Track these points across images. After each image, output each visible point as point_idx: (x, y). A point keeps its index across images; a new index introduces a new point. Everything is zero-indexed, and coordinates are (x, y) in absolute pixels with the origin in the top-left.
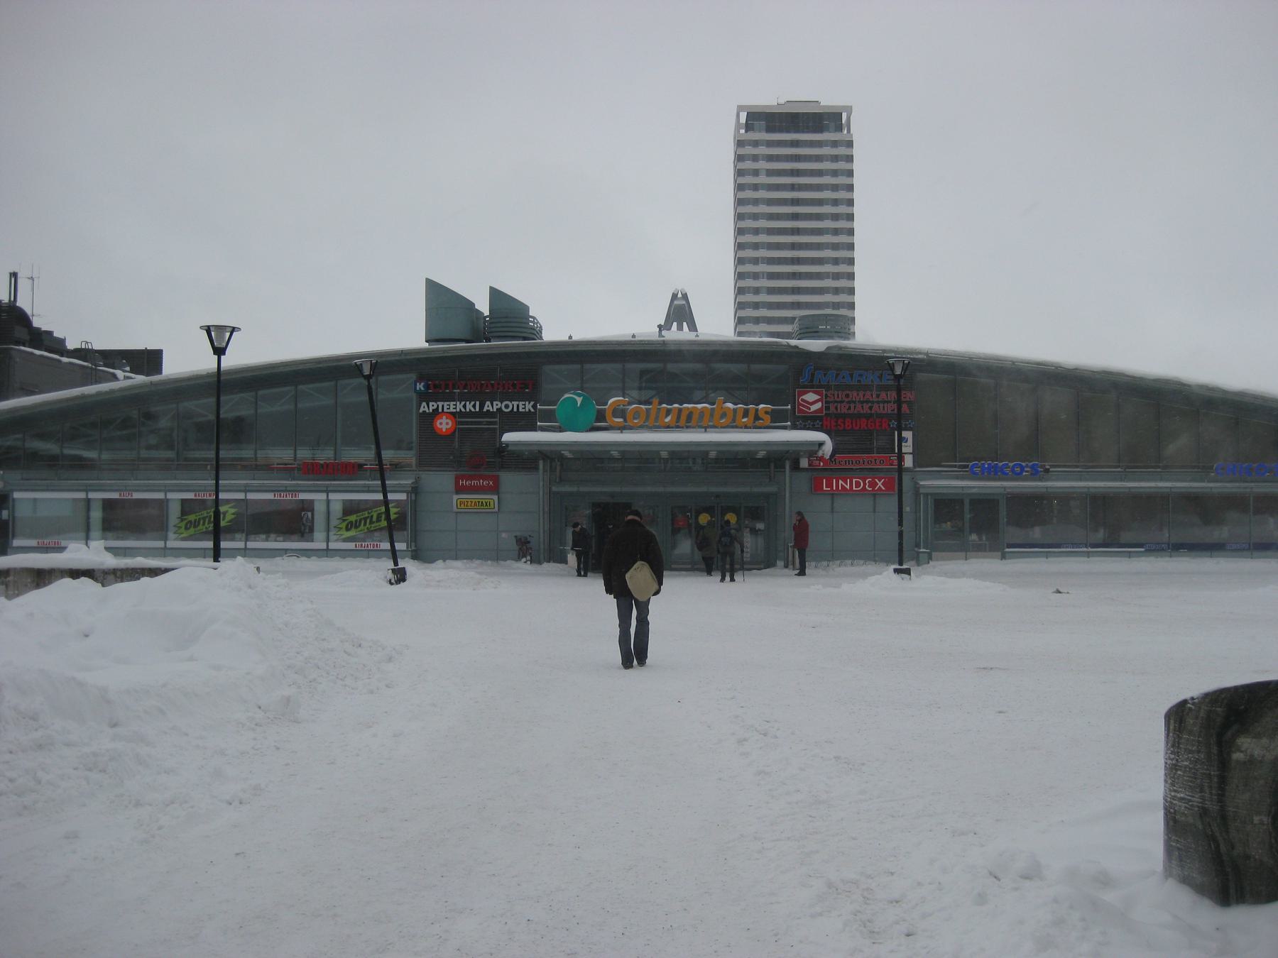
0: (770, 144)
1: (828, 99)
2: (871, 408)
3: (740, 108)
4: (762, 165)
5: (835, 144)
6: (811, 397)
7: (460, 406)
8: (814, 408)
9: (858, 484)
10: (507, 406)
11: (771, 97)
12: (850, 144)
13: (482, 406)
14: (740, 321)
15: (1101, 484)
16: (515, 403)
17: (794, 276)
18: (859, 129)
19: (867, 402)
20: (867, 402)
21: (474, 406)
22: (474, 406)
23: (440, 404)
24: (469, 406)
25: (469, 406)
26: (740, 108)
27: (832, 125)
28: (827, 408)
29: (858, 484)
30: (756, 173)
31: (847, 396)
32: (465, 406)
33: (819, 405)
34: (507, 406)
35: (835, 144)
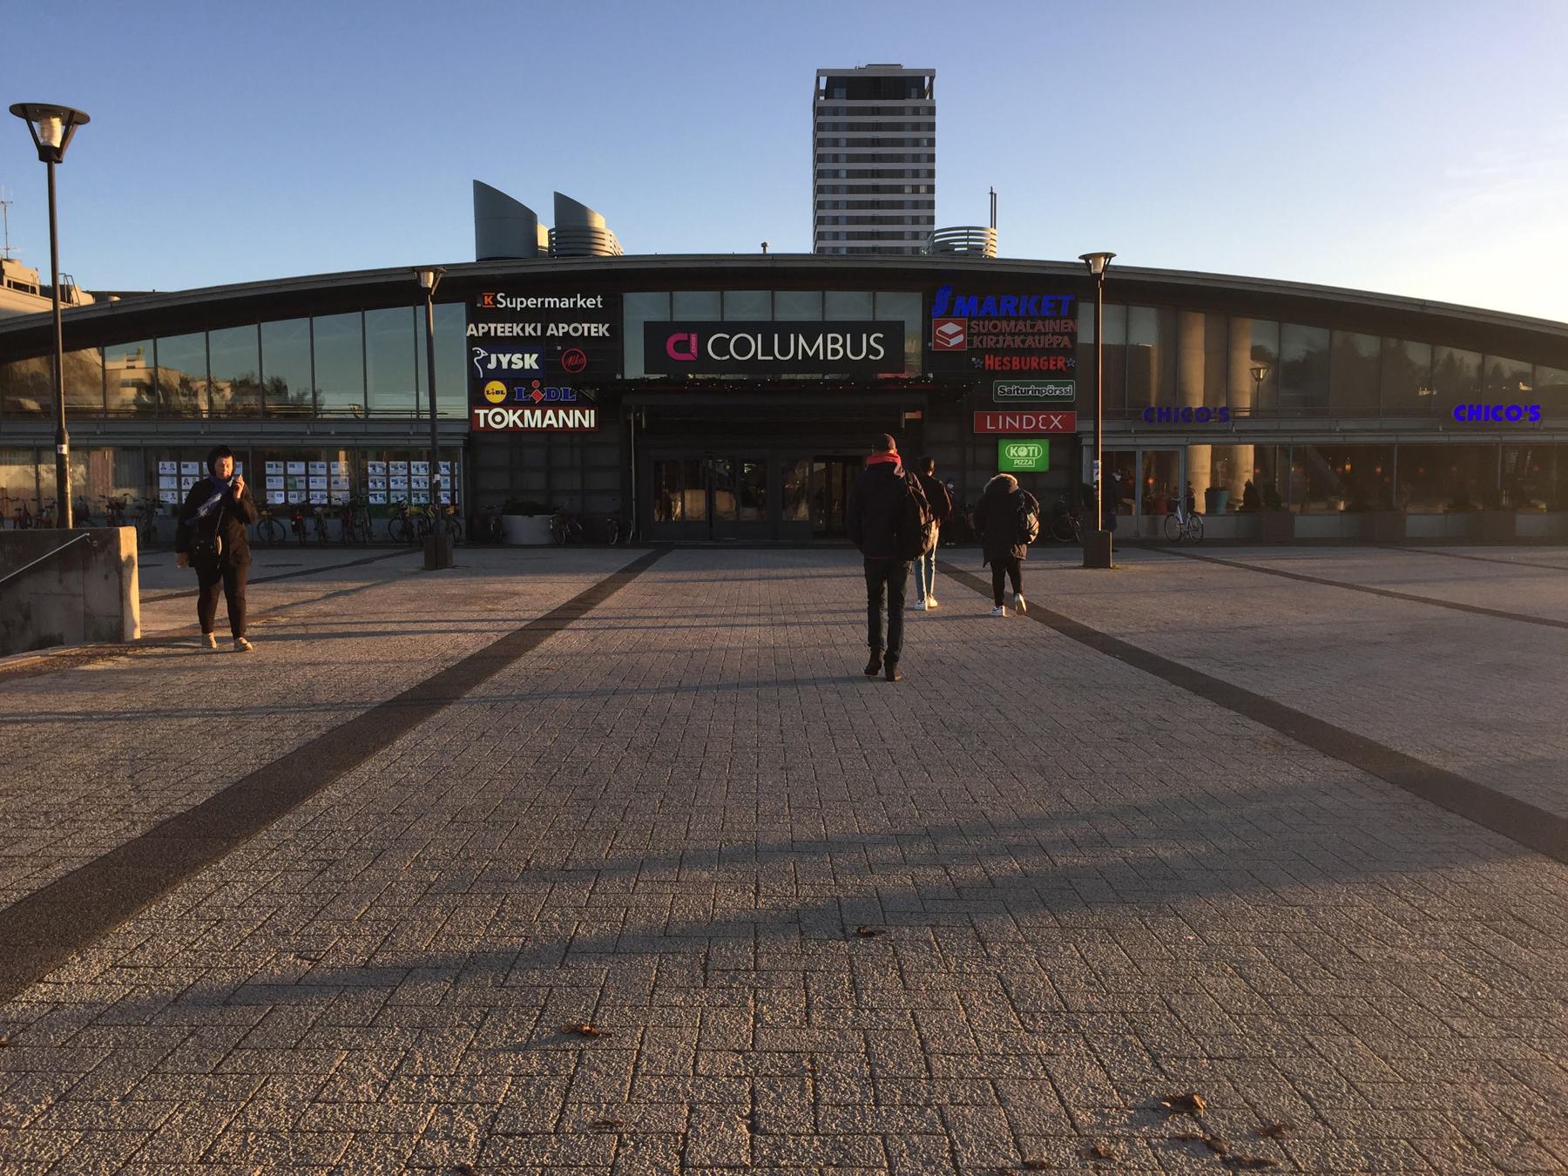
0: (851, 111)
1: (910, 60)
2: (1023, 342)
3: (820, 73)
4: (843, 166)
5: (916, 111)
6: (950, 328)
7: (517, 329)
8: (954, 342)
9: (1029, 422)
10: (576, 330)
11: (851, 59)
12: (932, 111)
13: (544, 329)
14: (819, 236)
15: (1382, 439)
16: (586, 326)
17: (874, 220)
18: (942, 96)
19: (1020, 334)
20: (1020, 334)
21: (535, 329)
22: (535, 329)
23: (492, 326)
24: (529, 330)
25: (529, 330)
26: (820, 73)
27: (914, 91)
28: (970, 342)
29: (1029, 422)
30: (836, 174)
31: (995, 327)
32: (523, 329)
33: (960, 338)
34: (576, 330)
35: (916, 111)
